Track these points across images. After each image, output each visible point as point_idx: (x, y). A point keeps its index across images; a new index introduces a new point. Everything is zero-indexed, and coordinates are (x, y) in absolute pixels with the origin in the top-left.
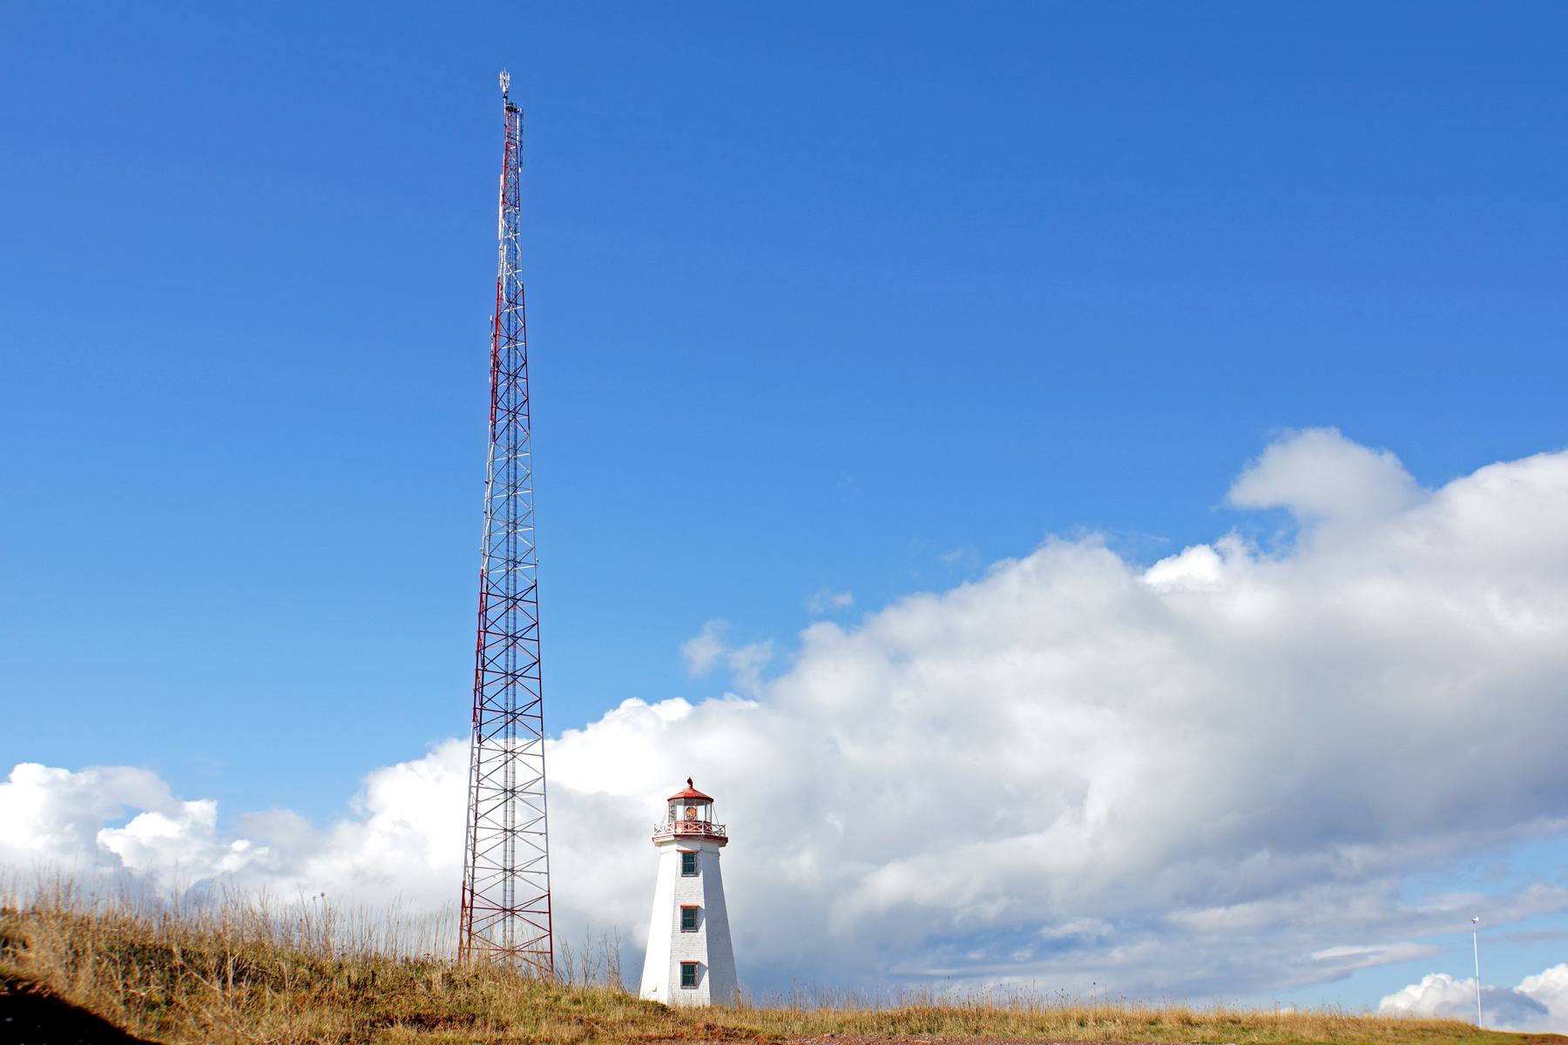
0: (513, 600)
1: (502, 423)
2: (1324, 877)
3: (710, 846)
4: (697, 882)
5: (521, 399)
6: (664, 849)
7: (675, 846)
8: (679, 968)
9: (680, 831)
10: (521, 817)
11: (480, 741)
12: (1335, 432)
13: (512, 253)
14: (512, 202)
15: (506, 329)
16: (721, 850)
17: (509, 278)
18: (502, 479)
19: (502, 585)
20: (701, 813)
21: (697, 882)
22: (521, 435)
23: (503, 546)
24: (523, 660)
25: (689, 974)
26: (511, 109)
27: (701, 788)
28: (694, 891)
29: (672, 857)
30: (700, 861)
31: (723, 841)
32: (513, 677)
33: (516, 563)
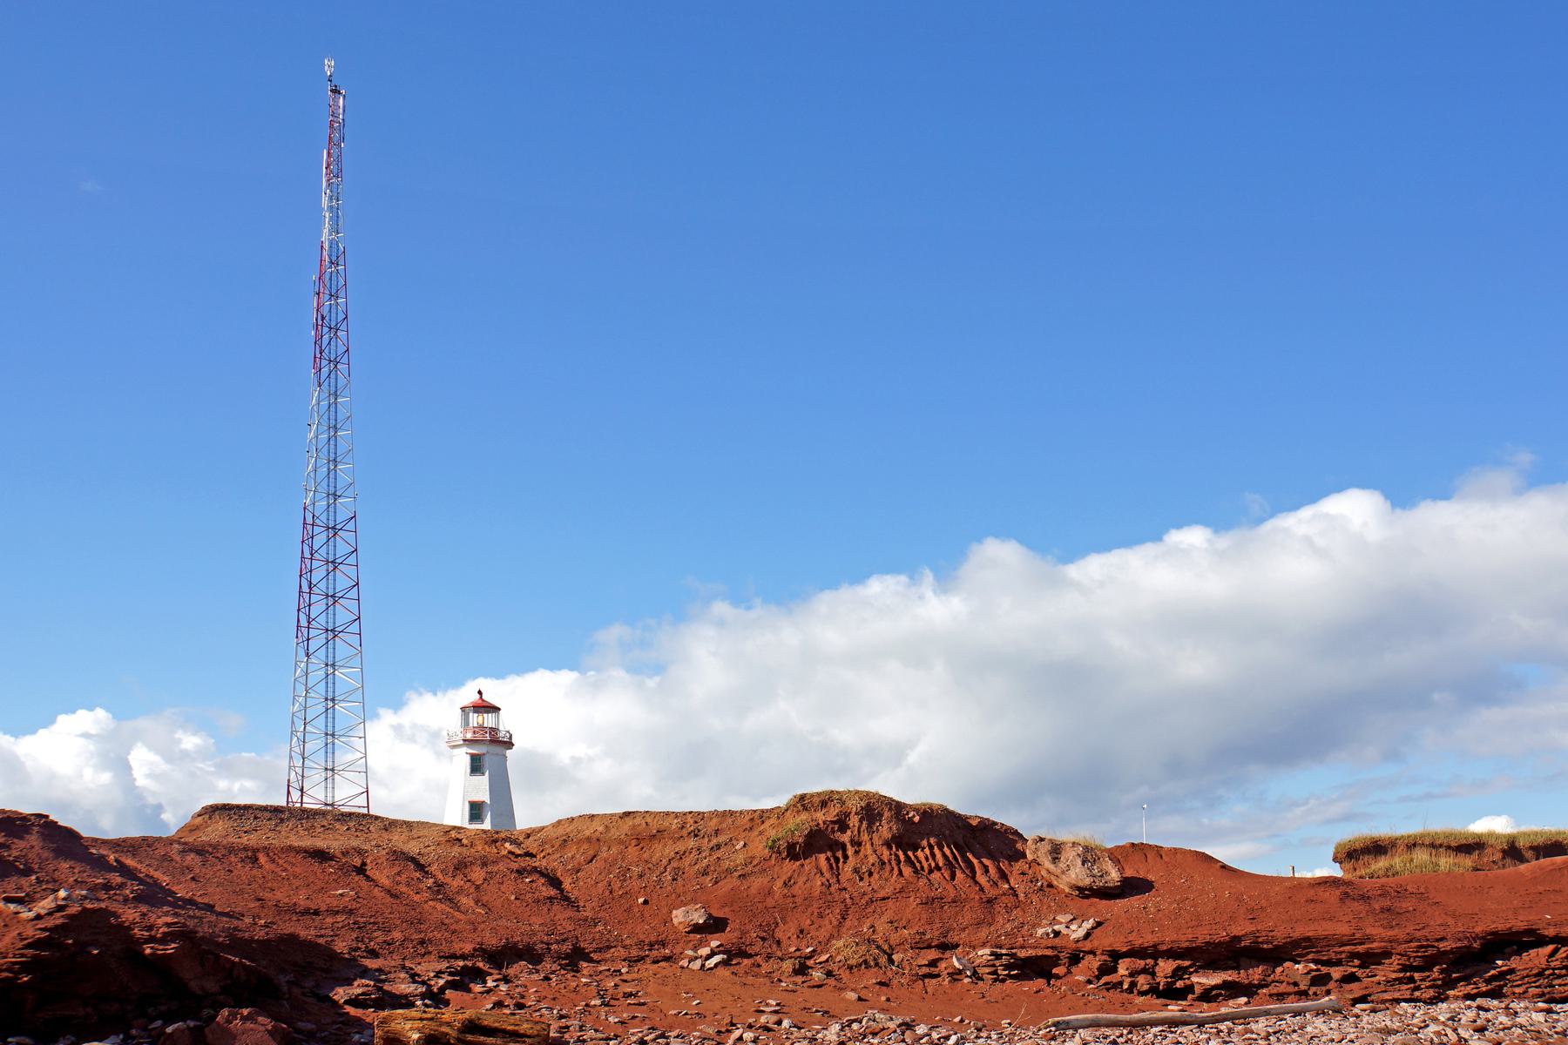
0: (333, 530)
1: (325, 371)
2: (1249, 990)
3: (496, 749)
4: (483, 781)
5: (342, 349)
6: (456, 751)
7: (465, 749)
8: (467, 806)
9: (469, 736)
10: (342, 549)
11: (308, 655)
12: (1429, 501)
13: (335, 219)
14: (336, 172)
15: (328, 288)
16: (508, 752)
17: (331, 242)
18: (323, 488)
19: (323, 518)
20: (489, 720)
21: (483, 781)
22: (342, 381)
23: (324, 484)
24: (342, 549)
25: (476, 811)
26: (336, 91)
27: (490, 698)
28: (481, 789)
29: (463, 757)
30: (487, 761)
31: (509, 745)
32: (333, 564)
33: (336, 497)
